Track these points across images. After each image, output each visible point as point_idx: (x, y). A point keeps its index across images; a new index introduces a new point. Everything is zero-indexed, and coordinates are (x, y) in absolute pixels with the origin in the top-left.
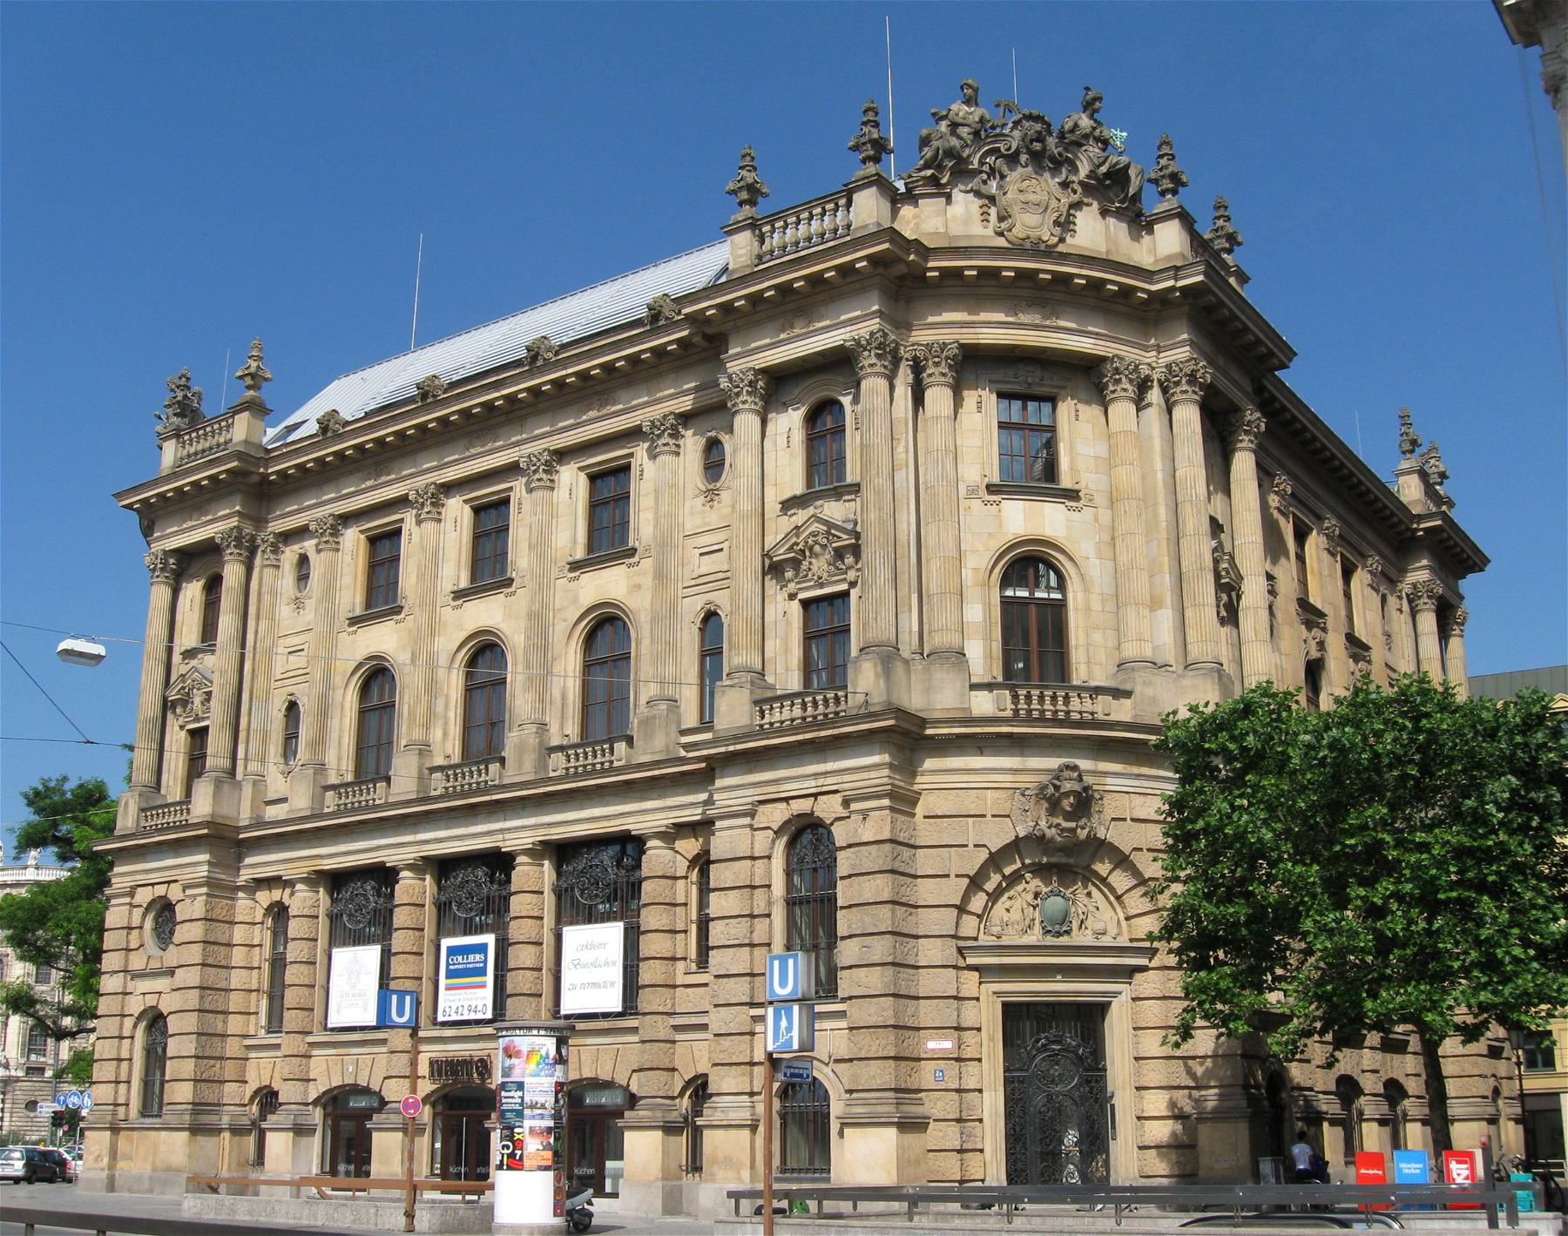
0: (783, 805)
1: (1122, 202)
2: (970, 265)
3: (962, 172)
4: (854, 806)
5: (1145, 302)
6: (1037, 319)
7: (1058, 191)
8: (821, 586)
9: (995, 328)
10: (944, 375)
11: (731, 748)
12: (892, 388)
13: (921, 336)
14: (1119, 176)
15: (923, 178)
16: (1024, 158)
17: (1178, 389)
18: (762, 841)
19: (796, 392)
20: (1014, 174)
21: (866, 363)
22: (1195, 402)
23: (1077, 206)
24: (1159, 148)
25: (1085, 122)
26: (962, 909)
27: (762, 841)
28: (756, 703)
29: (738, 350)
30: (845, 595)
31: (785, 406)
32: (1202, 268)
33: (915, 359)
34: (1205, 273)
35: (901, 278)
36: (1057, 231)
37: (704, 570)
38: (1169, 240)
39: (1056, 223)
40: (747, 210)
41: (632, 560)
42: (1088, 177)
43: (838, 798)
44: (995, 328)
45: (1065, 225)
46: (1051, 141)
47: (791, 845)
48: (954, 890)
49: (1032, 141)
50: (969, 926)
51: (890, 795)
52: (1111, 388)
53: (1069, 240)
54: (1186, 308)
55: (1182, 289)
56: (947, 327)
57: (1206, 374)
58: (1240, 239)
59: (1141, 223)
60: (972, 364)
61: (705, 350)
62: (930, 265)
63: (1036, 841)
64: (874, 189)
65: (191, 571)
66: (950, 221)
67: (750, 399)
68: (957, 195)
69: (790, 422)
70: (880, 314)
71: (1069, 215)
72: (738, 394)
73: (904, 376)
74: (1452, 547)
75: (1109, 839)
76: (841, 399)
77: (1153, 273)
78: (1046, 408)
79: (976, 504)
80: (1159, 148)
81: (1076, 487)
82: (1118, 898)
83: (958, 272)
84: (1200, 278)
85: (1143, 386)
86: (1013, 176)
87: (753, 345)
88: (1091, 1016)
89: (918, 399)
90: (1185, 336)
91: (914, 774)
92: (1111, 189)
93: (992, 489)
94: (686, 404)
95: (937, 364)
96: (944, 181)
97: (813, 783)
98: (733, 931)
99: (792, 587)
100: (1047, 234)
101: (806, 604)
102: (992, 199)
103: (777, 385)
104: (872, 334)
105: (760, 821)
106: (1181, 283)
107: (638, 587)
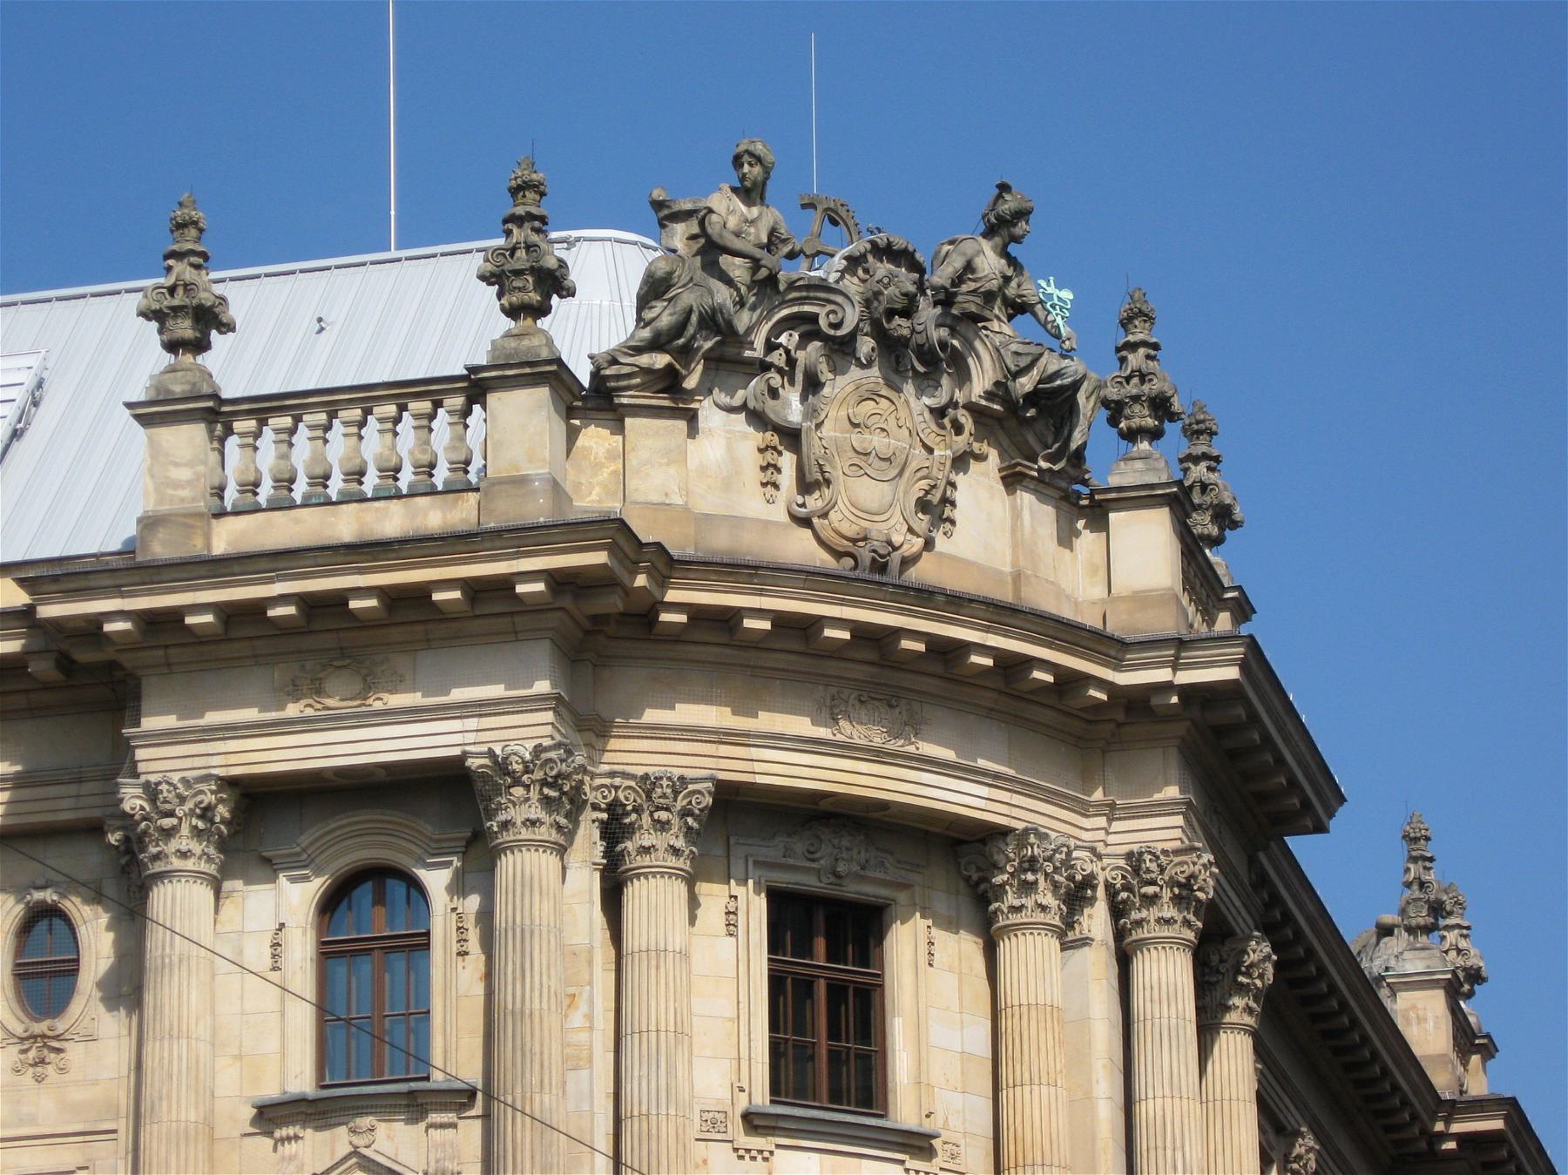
1: (1052, 459)
2: (758, 606)
3: (729, 361)
5: (1098, 706)
6: (876, 736)
7: (926, 425)
9: (793, 749)
10: (676, 852)
14: (1056, 404)
15: (647, 371)
17: (1152, 914)
19: (305, 840)
20: (841, 380)
21: (517, 814)
22: (1185, 944)
23: (961, 462)
24: (1126, 323)
25: (990, 263)
29: (169, 721)
31: (268, 868)
32: (1238, 651)
33: (614, 808)
34: (1244, 666)
36: (922, 522)
38: (1144, 549)
39: (923, 505)
42: (989, 395)
44: (793, 749)
45: (936, 509)
46: (928, 312)
49: (891, 313)
52: (1011, 899)
53: (941, 543)
54: (1181, 728)
55: (1187, 691)
56: (687, 738)
57: (1202, 867)
58: (1238, 513)
59: (1085, 507)
61: (47, 687)
62: (672, 596)
64: (543, 393)
67: (196, 847)
68: (709, 414)
69: (291, 901)
70: (557, 703)
72: (169, 833)
73: (588, 843)
74: (1391, 1112)
76: (424, 875)
77: (1123, 645)
79: (720, 1154)
80: (1126, 323)
81: (927, 1126)
83: (728, 618)
84: (1232, 673)
85: (1076, 896)
86: (840, 386)
87: (213, 718)
90: (1172, 792)
92: (1034, 432)
93: (753, 1122)
95: (662, 826)
96: (691, 383)
100: (897, 528)
102: (791, 437)
103: (261, 819)
104: (538, 750)
106: (1185, 677)
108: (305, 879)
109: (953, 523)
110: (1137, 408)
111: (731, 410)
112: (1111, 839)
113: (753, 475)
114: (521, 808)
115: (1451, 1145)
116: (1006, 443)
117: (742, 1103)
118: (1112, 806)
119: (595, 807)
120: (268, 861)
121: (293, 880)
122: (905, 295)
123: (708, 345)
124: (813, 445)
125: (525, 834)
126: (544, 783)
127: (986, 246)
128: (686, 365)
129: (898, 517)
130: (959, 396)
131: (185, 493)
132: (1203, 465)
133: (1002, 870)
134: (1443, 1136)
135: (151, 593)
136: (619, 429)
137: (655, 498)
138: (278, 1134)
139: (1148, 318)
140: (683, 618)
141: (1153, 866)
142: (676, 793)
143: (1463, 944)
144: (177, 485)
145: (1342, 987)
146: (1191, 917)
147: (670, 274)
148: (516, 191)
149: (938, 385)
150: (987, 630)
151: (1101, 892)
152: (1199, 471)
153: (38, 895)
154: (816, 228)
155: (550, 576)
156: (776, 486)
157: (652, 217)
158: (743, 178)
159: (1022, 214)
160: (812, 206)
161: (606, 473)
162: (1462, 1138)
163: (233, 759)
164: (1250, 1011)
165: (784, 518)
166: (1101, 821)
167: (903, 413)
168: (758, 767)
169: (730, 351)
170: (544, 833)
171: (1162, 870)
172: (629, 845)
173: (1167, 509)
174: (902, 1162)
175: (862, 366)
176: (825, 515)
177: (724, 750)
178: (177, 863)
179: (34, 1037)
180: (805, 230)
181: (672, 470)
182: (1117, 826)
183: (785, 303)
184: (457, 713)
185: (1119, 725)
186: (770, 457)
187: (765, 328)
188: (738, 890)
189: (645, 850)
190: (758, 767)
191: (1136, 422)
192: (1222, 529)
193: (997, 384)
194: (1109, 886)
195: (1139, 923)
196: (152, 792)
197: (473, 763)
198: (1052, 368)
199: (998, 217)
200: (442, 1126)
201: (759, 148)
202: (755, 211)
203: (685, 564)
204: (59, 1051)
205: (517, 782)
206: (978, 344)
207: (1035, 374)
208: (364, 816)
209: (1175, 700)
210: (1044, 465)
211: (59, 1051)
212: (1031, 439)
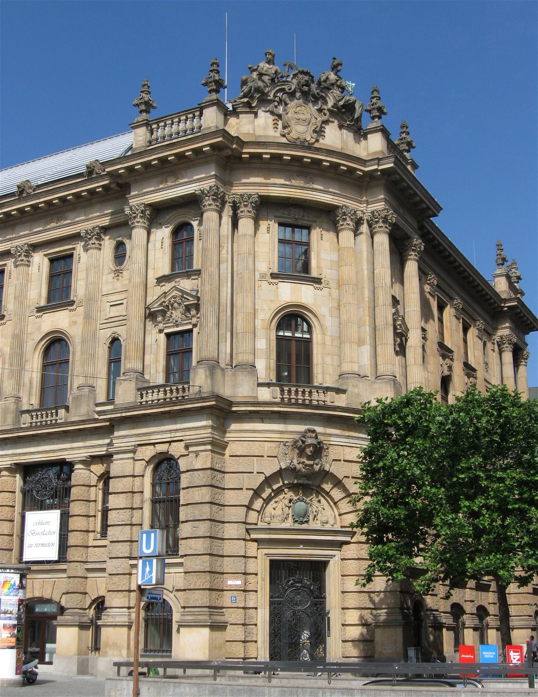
0: (151, 447)
1: (351, 121)
2: (266, 152)
3: (264, 100)
4: (191, 449)
7: (316, 114)
8: (177, 326)
9: (279, 187)
10: (249, 212)
11: (124, 415)
12: (220, 218)
13: (238, 190)
14: (349, 107)
15: (242, 103)
16: (298, 95)
17: (378, 225)
18: (139, 467)
19: (167, 218)
21: (207, 203)
22: (386, 232)
23: (326, 122)
24: (372, 93)
25: (332, 77)
26: (249, 508)
27: (139, 467)
28: (138, 390)
30: (190, 331)
31: (161, 225)
32: (393, 160)
34: (395, 163)
35: (228, 157)
36: (315, 135)
37: (112, 315)
39: (315, 131)
40: (144, 116)
41: (72, 308)
42: (333, 107)
43: (182, 444)
45: (319, 132)
46: (314, 86)
47: (155, 469)
48: (245, 497)
49: (303, 86)
50: (253, 517)
51: (212, 443)
52: (341, 223)
53: (321, 141)
54: (383, 181)
55: (382, 171)
58: (414, 144)
59: (360, 134)
60: (265, 206)
61: (117, 192)
62: (245, 151)
63: (292, 471)
64: (215, 107)
65: (161, 221)
66: (256, 127)
67: (141, 221)
68: (261, 113)
69: (163, 234)
71: (321, 127)
72: (135, 218)
73: (228, 211)
75: (331, 471)
76: (192, 222)
77: (366, 161)
78: (305, 232)
79: (265, 284)
80: (372, 93)
81: (320, 277)
82: (335, 503)
83: (259, 156)
84: (392, 165)
85: (358, 223)
86: (292, 104)
87: (145, 191)
88: (318, 568)
89: (235, 225)
91: (225, 432)
92: (345, 114)
94: (105, 221)
95: (246, 206)
97: (169, 435)
98: (122, 517)
99: (161, 326)
100: (309, 137)
101: (168, 335)
102: (280, 116)
103: (157, 213)
104: (211, 187)
105: (138, 456)
106: (381, 168)
107: (75, 323)
108: (168, 227)
109: (324, 136)
110: (374, 111)
111: (266, 112)
112: (368, 209)
113: (271, 126)
114: (208, 201)
115: (506, 309)
116: (339, 119)
117: (271, 271)
118: (367, 201)
119: (230, 203)
120: (160, 224)
121: (166, 227)
122: (306, 81)
123: (258, 96)
124: (285, 117)
125: (208, 207)
126: (213, 195)
127: (332, 73)
128: (253, 101)
129: (308, 134)
130: (325, 107)
131: (141, 143)
132: (404, 134)
133: (339, 216)
134: (504, 307)
135: (128, 162)
136: (238, 118)
137: (246, 132)
138: (161, 285)
139: (377, 91)
140: (248, 156)
141: (377, 214)
142: (249, 199)
143: (516, 271)
144: (140, 141)
145: (463, 264)
146: (388, 226)
147: (247, 79)
148: (212, 64)
149: (318, 104)
150: (327, 156)
151: (365, 222)
152: (404, 135)
153: (118, 239)
154: (287, 70)
155: (210, 145)
156: (277, 128)
157: (249, 71)
158: (267, 58)
159: (340, 64)
160: (285, 65)
161: (235, 128)
162: (508, 307)
163: (148, 200)
164: (416, 255)
165: (279, 135)
166: (365, 205)
167: (308, 110)
168: (270, 191)
169: (265, 98)
170: (213, 207)
171: (379, 215)
172: (239, 211)
173: (380, 133)
174: (313, 285)
175: (298, 99)
176: (289, 134)
177: (262, 188)
178: (136, 224)
179: (116, 270)
180: (284, 71)
181: (251, 126)
182: (369, 206)
183: (277, 86)
184: (194, 182)
185: (369, 182)
186: (275, 122)
187: (273, 92)
188: (269, 222)
189: (242, 212)
190: (270, 191)
191: (374, 114)
192: (409, 148)
193: (334, 104)
194: (367, 220)
195: (374, 228)
196: (131, 209)
197: (197, 192)
198: (347, 99)
199: (334, 66)
200: (194, 279)
201: (270, 51)
202: (271, 66)
203: (247, 143)
204: (121, 273)
205: (207, 196)
206: (329, 94)
207: (344, 100)
208: (180, 210)
209: (379, 173)
210: (348, 123)
211: (121, 273)
212: (345, 117)
